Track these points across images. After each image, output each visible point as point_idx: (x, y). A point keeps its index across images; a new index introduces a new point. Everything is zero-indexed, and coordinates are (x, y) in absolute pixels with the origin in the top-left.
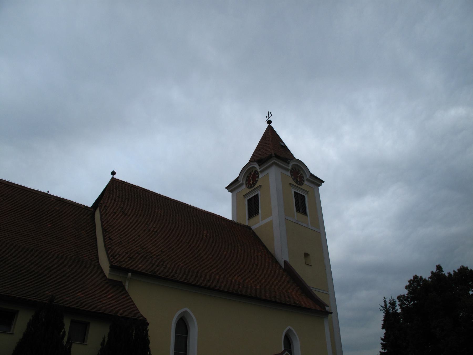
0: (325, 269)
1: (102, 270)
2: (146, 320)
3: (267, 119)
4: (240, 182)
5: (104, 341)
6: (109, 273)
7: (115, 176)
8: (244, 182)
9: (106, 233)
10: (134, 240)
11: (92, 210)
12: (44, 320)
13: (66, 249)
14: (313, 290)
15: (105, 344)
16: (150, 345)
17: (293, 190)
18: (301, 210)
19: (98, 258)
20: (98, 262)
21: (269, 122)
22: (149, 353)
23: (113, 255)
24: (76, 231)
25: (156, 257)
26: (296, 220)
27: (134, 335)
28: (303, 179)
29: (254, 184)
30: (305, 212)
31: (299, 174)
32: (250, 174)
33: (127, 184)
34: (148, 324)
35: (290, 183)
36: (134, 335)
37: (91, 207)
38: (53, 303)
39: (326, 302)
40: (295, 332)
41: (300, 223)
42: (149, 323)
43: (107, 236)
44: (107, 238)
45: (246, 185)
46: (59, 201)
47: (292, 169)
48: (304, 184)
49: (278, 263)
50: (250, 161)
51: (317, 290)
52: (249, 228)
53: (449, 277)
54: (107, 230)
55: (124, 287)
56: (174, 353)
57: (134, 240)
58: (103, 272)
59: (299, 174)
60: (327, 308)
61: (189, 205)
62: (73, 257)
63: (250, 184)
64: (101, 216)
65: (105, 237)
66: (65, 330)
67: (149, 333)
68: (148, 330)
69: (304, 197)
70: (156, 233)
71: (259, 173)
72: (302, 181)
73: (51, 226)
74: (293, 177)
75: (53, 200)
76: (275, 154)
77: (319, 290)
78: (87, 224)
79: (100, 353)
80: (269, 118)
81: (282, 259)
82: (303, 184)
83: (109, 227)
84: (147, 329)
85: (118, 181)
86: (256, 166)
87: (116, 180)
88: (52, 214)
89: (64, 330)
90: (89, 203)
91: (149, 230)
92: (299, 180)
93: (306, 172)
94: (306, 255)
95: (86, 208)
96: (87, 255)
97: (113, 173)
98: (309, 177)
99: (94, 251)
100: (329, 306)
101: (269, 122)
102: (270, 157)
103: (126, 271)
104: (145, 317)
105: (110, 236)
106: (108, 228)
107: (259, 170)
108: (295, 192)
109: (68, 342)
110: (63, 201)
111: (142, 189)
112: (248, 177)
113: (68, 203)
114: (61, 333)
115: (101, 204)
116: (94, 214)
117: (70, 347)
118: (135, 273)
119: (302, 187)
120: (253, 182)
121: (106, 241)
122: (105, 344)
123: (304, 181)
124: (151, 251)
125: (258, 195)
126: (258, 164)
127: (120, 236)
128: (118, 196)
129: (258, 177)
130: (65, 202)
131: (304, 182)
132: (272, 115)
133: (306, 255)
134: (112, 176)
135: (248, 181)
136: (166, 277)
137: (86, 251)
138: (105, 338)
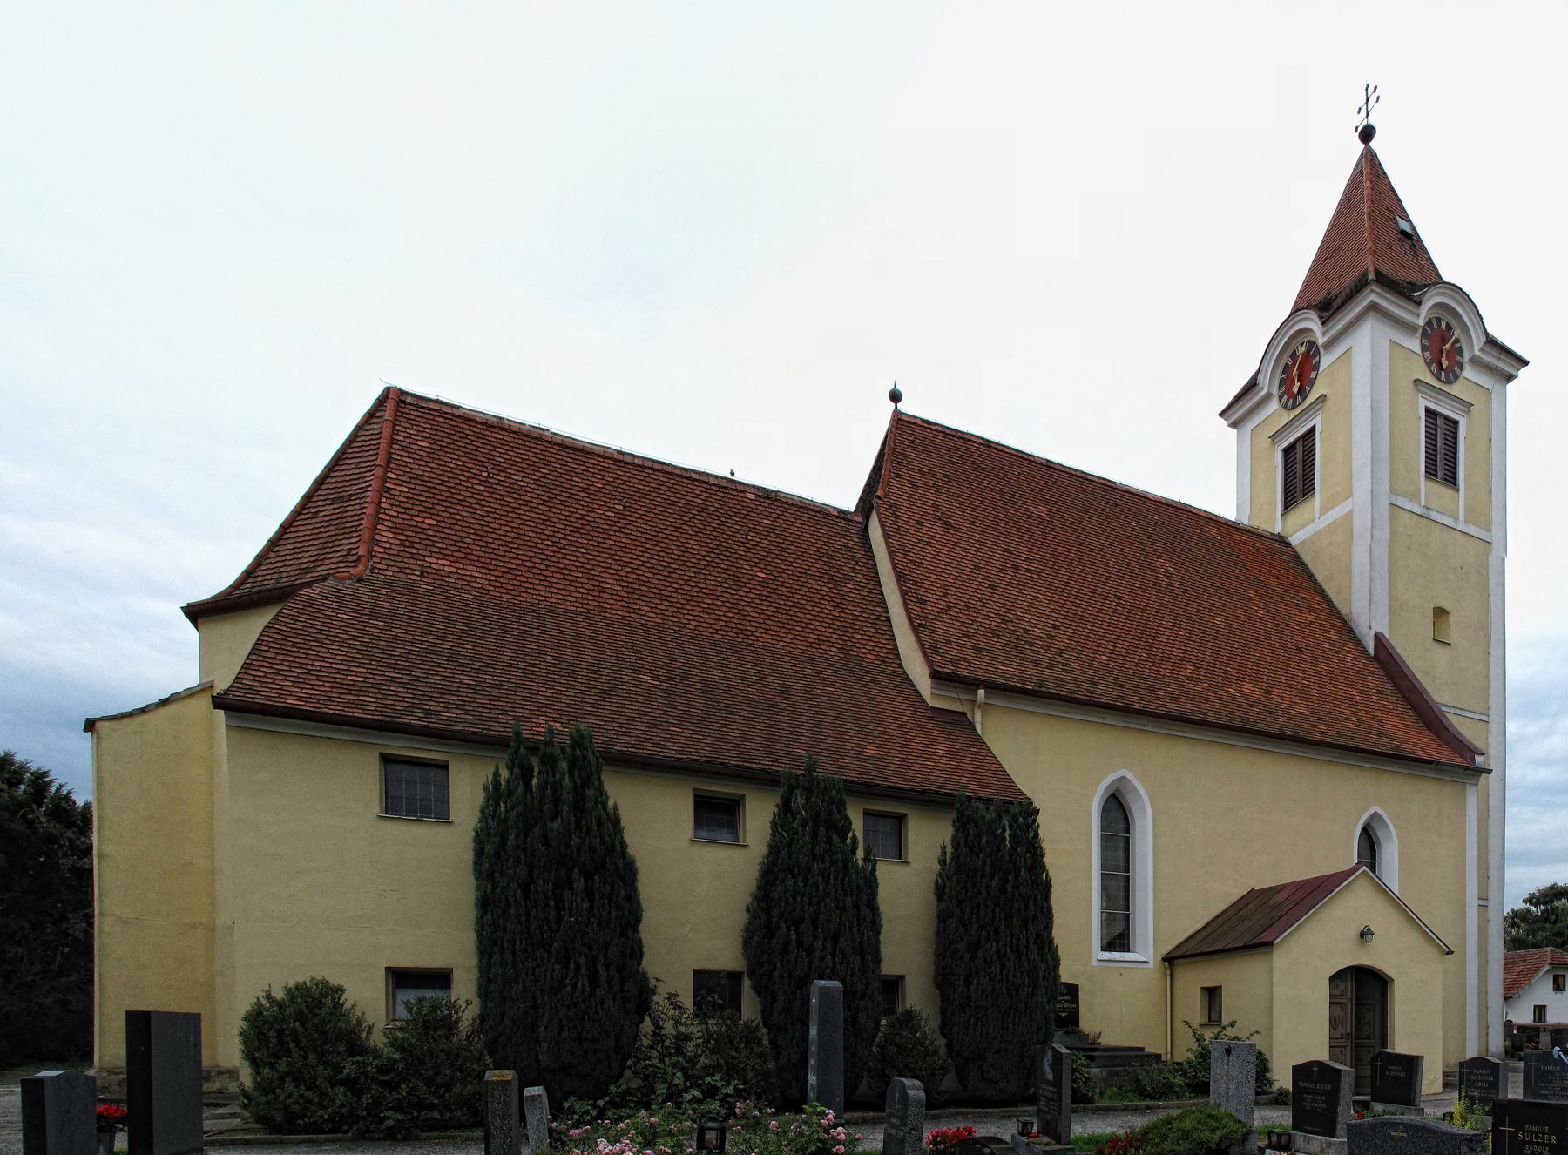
0: (1489, 653)
2: (1032, 803)
3: (1360, 122)
4: (1263, 388)
5: (944, 852)
7: (902, 407)
8: (1275, 391)
10: (981, 600)
11: (859, 519)
14: (1446, 714)
15: (948, 861)
17: (1423, 403)
18: (1439, 473)
19: (898, 656)
20: (901, 665)
21: (1367, 134)
26: (1423, 504)
27: (1007, 837)
28: (1458, 358)
29: (1303, 393)
30: (1451, 480)
32: (1294, 356)
34: (1037, 812)
35: (1416, 378)
36: (1007, 837)
37: (855, 511)
38: (816, 774)
39: (1479, 744)
40: (1388, 821)
41: (1434, 515)
42: (1039, 810)
43: (910, 594)
44: (912, 599)
45: (1280, 398)
46: (768, 501)
47: (1429, 323)
48: (1460, 380)
49: (1358, 642)
50: (1296, 310)
51: (1458, 712)
52: (1282, 541)
54: (909, 577)
55: (971, 725)
57: (981, 600)
58: (917, 692)
60: (1479, 759)
63: (1289, 392)
64: (886, 536)
65: (907, 597)
66: (856, 833)
68: (1039, 825)
69: (1456, 423)
70: (1034, 576)
71: (1322, 350)
72: (1456, 368)
73: (764, 576)
74: (1427, 354)
75: (753, 497)
76: (1377, 272)
77: (1464, 713)
80: (1368, 113)
81: (1370, 628)
82: (1457, 378)
85: (914, 421)
86: (1312, 322)
91: (1017, 568)
92: (1445, 363)
93: (1473, 334)
94: (1440, 613)
97: (895, 397)
98: (1482, 350)
100: (1484, 751)
101: (1367, 134)
102: (1360, 286)
103: (972, 684)
106: (910, 571)
107: (1321, 340)
108: (1429, 411)
109: (866, 859)
112: (1286, 369)
113: (794, 505)
114: (849, 841)
117: (874, 870)
118: (991, 687)
119: (1456, 389)
120: (1300, 388)
121: (910, 606)
122: (948, 861)
123: (1461, 366)
124: (1028, 628)
125: (1313, 430)
126: (1321, 318)
127: (944, 591)
128: (920, 472)
129: (1316, 367)
132: (1378, 98)
133: (1440, 613)
134: (892, 405)
135: (1285, 383)
138: (945, 847)
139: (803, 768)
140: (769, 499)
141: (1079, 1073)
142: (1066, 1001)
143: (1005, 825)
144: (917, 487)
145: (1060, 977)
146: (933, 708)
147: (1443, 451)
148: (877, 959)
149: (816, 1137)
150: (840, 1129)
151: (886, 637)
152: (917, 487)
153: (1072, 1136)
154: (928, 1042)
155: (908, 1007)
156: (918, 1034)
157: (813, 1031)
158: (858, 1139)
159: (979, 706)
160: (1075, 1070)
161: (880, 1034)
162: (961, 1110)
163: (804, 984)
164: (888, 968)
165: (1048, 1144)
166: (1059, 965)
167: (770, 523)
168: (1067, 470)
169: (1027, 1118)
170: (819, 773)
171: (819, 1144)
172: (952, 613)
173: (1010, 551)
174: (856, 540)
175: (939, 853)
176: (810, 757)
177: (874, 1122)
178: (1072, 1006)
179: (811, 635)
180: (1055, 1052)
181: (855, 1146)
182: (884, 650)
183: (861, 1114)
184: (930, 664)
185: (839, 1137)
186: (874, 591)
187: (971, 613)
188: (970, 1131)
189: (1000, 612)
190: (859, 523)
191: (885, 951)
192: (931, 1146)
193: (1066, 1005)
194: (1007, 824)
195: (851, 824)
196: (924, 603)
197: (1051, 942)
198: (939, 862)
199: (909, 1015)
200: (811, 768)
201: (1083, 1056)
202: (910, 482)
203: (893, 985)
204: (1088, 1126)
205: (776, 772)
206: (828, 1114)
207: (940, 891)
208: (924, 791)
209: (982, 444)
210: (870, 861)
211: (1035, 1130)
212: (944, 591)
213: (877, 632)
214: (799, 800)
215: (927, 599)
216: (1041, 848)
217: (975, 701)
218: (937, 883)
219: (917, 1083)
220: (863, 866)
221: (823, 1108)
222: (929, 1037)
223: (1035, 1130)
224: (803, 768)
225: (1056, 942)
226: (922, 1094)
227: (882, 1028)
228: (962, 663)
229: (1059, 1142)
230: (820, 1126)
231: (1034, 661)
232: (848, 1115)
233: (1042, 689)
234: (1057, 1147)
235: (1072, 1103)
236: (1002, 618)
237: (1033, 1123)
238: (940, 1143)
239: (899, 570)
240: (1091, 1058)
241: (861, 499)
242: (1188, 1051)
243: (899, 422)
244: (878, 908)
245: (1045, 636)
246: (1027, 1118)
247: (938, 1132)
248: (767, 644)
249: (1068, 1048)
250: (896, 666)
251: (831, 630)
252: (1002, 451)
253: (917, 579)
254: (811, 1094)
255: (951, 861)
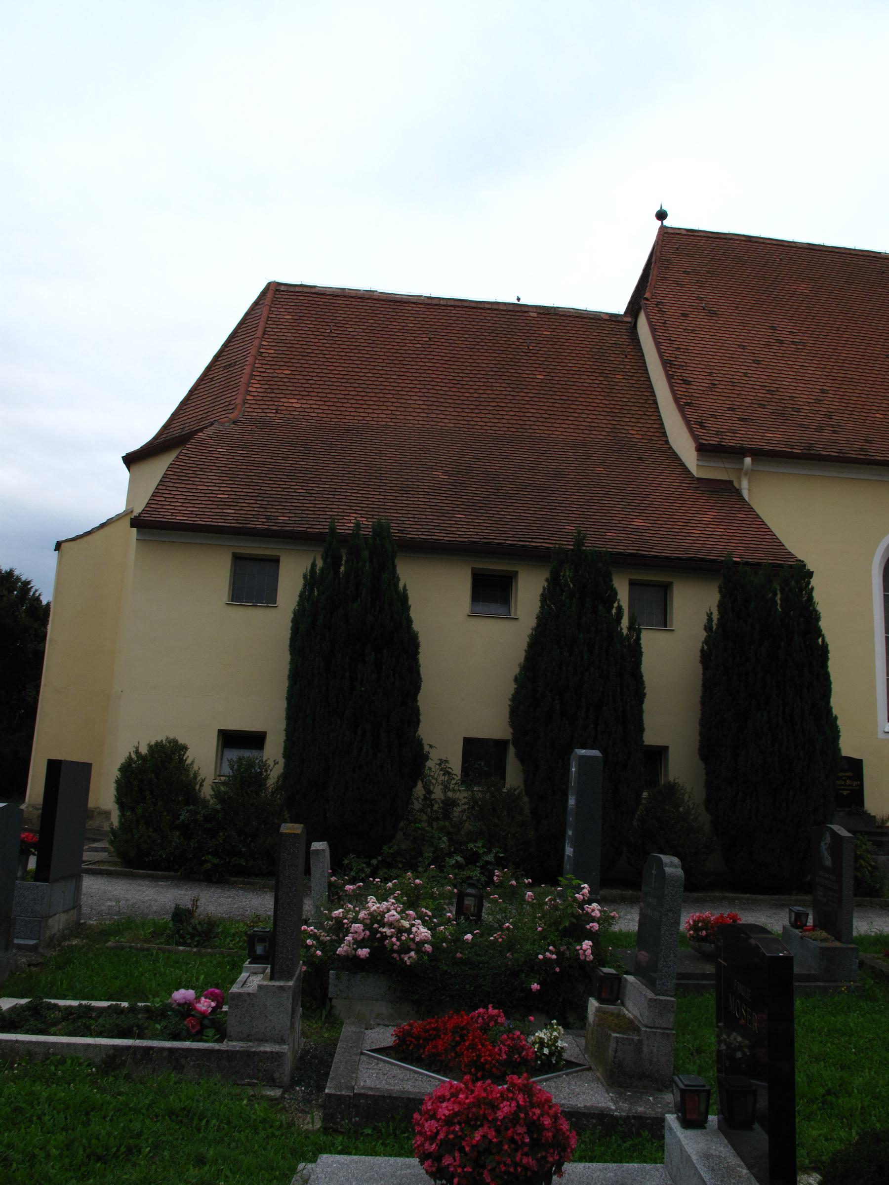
1: (680, 460)
2: (805, 566)
5: (710, 619)
6: (698, 465)
7: (667, 223)
9: (673, 370)
10: (745, 374)
11: (629, 319)
12: (571, 585)
13: (588, 424)
15: (715, 627)
16: (820, 623)
19: (664, 434)
20: (667, 442)
22: (820, 640)
23: (700, 420)
24: (602, 379)
25: (809, 408)
27: (779, 602)
33: (702, 234)
34: (810, 574)
36: (779, 602)
38: (584, 548)
42: (813, 572)
43: (676, 377)
46: (548, 316)
55: (738, 492)
56: (884, 595)
57: (745, 374)
61: (880, 253)
62: (606, 441)
64: (653, 330)
65: (673, 381)
66: (622, 603)
67: (815, 594)
68: (812, 588)
70: (799, 347)
75: (535, 315)
78: (624, 356)
79: (706, 647)
83: (676, 353)
84: (810, 587)
85: (679, 232)
87: (672, 231)
88: (538, 349)
89: (619, 604)
90: (618, 304)
91: (781, 342)
95: (613, 318)
96: (639, 429)
97: (661, 215)
99: (653, 418)
103: (738, 453)
104: (800, 557)
105: (683, 374)
106: (676, 358)
110: (555, 314)
111: (744, 239)
113: (570, 316)
114: (614, 611)
115: (647, 299)
116: (636, 329)
117: (638, 638)
118: (759, 454)
121: (676, 388)
122: (715, 627)
127: (709, 371)
128: (684, 272)
130: (563, 315)
134: (659, 223)
136: (841, 455)
137: (633, 420)
138: (711, 614)
139: (571, 543)
140: (548, 314)
141: (864, 860)
142: (848, 778)
143: (776, 589)
144: (682, 286)
145: (839, 750)
146: (699, 479)
148: (641, 729)
149: (569, 911)
150: (595, 905)
151: (653, 418)
152: (682, 286)
153: (855, 934)
154: (692, 817)
155: (671, 779)
156: (681, 809)
157: (572, 801)
158: (613, 918)
159: (746, 474)
160: (857, 858)
161: (641, 807)
162: (727, 894)
163: (565, 753)
164: (651, 738)
165: (825, 940)
166: (838, 737)
167: (549, 333)
168: (830, 250)
169: (801, 908)
170: (588, 546)
171: (574, 920)
172: (717, 390)
173: (774, 328)
174: (625, 337)
175: (704, 619)
176: (579, 533)
177: (631, 901)
178: (855, 783)
179: (583, 424)
180: (834, 834)
181: (610, 925)
182: (652, 430)
183: (619, 892)
184: (695, 438)
185: (593, 914)
186: (642, 379)
187: (736, 388)
188: (734, 918)
189: (765, 384)
190: (628, 322)
191: (649, 720)
192: (692, 932)
193: (848, 782)
194: (778, 587)
195: (616, 594)
196: (688, 383)
197: (829, 710)
198: (705, 629)
199: (672, 788)
200: (580, 541)
201: (869, 841)
202: (675, 282)
203: (658, 754)
204: (875, 923)
205: (548, 548)
206: (584, 888)
207: (706, 658)
208: (690, 559)
209: (743, 241)
210: (635, 629)
211: (810, 922)
212: (709, 371)
213: (645, 414)
214: (567, 574)
215: (692, 380)
216: (816, 611)
217: (741, 469)
218: (702, 651)
219: (676, 860)
220: (627, 635)
221: (580, 882)
222: (693, 812)
223: (810, 922)
224: (571, 543)
225: (835, 712)
226: (680, 872)
227: (644, 801)
228: (727, 434)
229: (838, 939)
230: (575, 899)
231: (802, 426)
232: (604, 892)
233: (812, 452)
234: (837, 944)
235: (855, 895)
236: (767, 388)
237: (807, 915)
238: (701, 929)
239: (666, 358)
240: (879, 844)
241: (630, 303)
243: (666, 235)
244: (641, 676)
245: (813, 401)
246: (801, 908)
247: (699, 917)
248: (543, 435)
249: (849, 831)
250: (663, 443)
251: (601, 417)
252: (763, 243)
253: (682, 364)
254: (567, 866)
255: (718, 625)
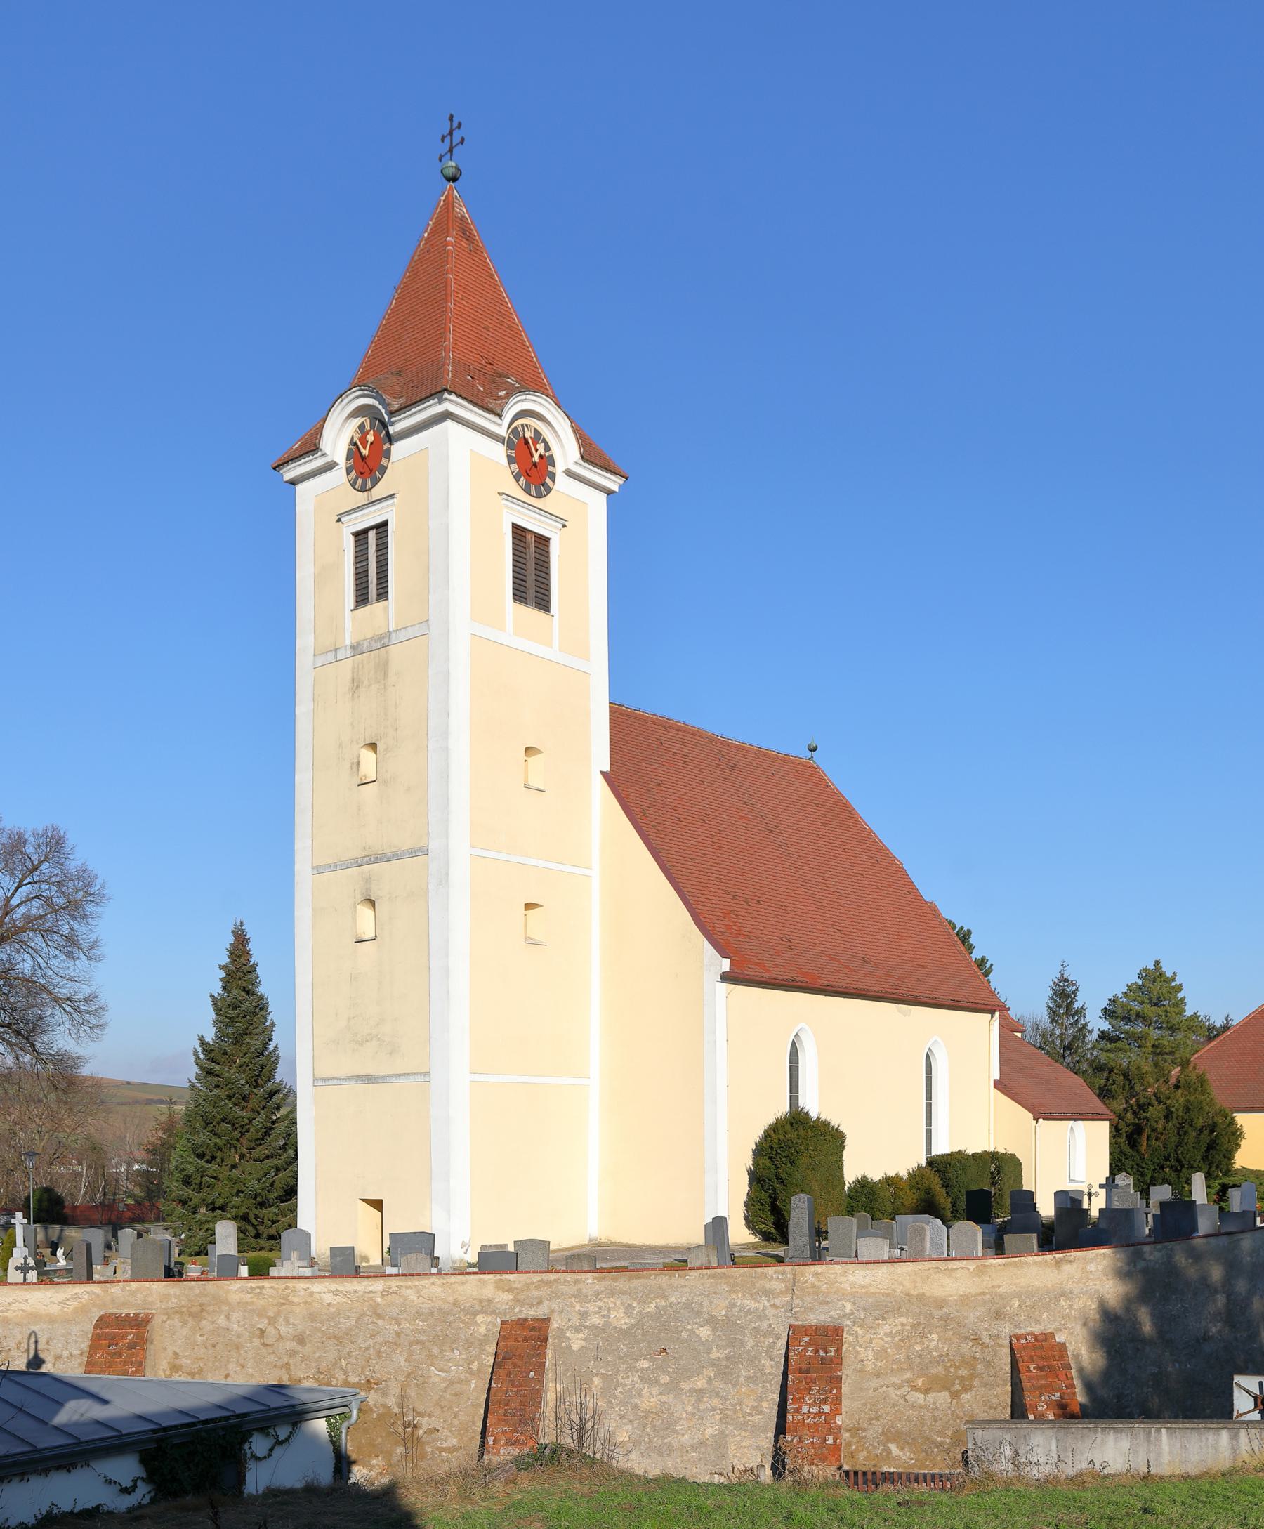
28: (550, 468)
30: (543, 603)
31: (515, 440)
45: (348, 471)
53: (350, 1487)
59: (515, 440)
74: (515, 466)
82: (549, 490)
119: (547, 503)
123: (553, 477)
131: (553, 479)
147: (528, 557)
242: (443, 140)
